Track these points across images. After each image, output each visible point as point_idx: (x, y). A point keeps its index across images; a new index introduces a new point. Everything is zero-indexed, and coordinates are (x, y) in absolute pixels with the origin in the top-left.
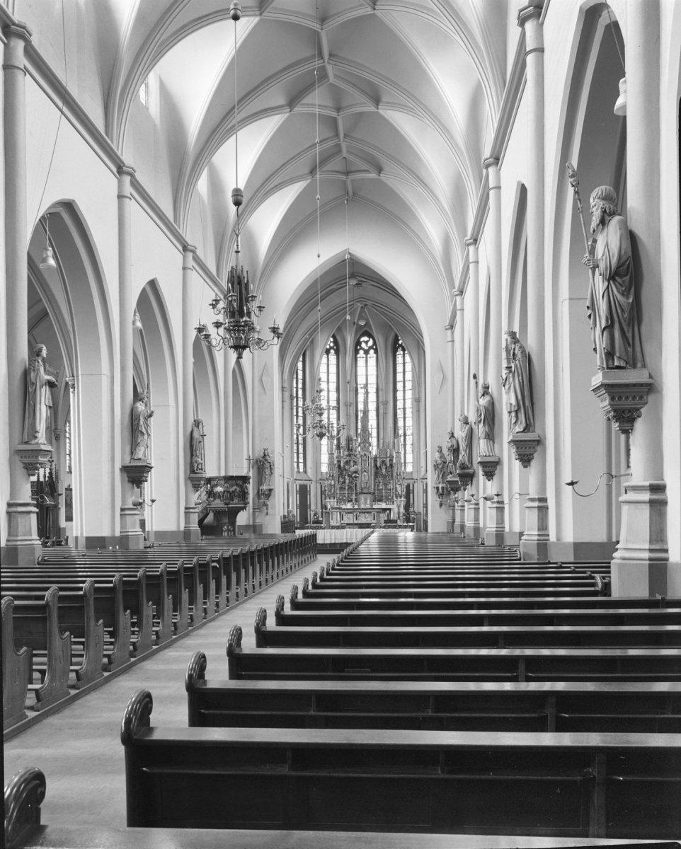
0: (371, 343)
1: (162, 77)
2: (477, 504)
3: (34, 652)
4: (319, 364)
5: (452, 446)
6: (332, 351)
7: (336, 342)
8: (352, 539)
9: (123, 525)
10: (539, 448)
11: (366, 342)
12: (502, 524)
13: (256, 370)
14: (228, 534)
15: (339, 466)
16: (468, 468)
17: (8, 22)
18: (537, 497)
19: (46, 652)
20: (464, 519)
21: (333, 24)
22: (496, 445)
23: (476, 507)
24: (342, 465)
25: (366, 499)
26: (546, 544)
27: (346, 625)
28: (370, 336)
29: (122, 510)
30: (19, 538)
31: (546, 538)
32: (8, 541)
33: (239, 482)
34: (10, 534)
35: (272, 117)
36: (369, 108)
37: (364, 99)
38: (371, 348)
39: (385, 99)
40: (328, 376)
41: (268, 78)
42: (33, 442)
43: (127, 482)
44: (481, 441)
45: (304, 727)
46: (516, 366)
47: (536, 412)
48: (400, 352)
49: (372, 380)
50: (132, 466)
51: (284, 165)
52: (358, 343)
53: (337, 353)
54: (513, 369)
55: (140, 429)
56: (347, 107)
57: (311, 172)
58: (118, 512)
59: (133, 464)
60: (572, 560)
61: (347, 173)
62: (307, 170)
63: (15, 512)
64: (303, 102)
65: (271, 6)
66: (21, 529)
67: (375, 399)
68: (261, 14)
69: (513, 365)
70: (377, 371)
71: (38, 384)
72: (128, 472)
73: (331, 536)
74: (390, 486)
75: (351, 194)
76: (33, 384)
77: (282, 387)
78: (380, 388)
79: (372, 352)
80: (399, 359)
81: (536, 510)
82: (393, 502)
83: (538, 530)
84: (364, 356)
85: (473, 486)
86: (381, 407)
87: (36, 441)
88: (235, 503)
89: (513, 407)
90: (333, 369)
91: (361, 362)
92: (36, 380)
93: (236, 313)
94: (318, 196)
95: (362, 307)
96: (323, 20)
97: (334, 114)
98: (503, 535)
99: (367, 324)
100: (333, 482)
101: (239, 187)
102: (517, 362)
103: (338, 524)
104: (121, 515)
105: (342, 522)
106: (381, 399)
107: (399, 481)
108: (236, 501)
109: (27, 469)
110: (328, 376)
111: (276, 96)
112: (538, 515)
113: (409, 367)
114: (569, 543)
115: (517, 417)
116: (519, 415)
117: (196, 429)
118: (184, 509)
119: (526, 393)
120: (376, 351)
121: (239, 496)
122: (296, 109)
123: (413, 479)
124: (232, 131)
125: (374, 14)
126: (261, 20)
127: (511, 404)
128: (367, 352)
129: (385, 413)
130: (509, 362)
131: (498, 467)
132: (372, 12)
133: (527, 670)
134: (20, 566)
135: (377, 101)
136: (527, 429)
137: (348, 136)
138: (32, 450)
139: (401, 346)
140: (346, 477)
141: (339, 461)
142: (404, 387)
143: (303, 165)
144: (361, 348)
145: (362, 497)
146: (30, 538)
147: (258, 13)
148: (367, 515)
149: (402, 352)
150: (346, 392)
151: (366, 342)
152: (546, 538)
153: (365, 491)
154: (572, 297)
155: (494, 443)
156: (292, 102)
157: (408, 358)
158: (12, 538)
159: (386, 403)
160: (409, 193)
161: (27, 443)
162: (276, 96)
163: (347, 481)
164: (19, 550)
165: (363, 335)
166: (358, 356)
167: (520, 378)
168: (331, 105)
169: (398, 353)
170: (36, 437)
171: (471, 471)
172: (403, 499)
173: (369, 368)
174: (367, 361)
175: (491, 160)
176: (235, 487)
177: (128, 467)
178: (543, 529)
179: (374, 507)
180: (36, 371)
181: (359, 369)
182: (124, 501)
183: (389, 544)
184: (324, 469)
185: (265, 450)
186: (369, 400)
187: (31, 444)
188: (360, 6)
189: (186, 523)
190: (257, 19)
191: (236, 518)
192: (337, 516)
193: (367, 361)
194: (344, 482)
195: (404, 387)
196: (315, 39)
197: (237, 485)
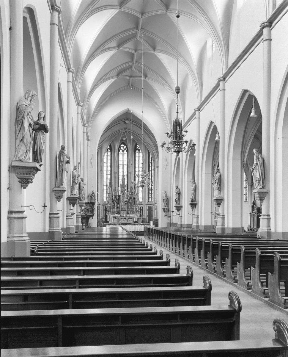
0: (125, 147)
1: (207, 41)
2: (182, 217)
3: (261, 275)
4: (104, 155)
5: (178, 192)
6: (109, 150)
7: (110, 146)
8: (137, 229)
9: (67, 223)
10: (267, 195)
11: (123, 147)
12: (224, 224)
13: (89, 157)
14: (85, 227)
15: (112, 199)
16: (194, 201)
17: (55, 5)
18: (266, 214)
19: (265, 275)
20: (198, 222)
21: (146, 16)
22: (221, 193)
23: (268, 217)
24: (114, 198)
25: (124, 213)
26: (270, 233)
27: (139, 266)
28: (125, 144)
29: (67, 216)
30: (55, 228)
31: (270, 230)
32: (49, 229)
33: (91, 205)
34: (50, 227)
35: (109, 52)
36: (151, 51)
37: (150, 47)
38: (125, 149)
39: (158, 48)
40: (107, 160)
41: (115, 35)
42: (61, 187)
43: (69, 204)
44: (216, 191)
45: (206, 305)
46: (260, 163)
47: (266, 181)
48: (137, 151)
49: (125, 163)
50: (72, 198)
51: (110, 71)
52: (120, 147)
53: (111, 151)
54: (258, 164)
55: (75, 182)
56: (140, 50)
57: (117, 75)
58: (65, 217)
59: (72, 196)
60: (282, 239)
61: (131, 77)
62: (116, 74)
63: (53, 217)
64: (124, 46)
65: (125, 6)
66: (55, 225)
67: (126, 171)
68: (120, 9)
69: (258, 162)
70: (128, 159)
71: (64, 162)
72: (69, 200)
73: (132, 228)
74: (134, 207)
75: (130, 85)
76: (62, 162)
77: (158, 168)
78: (129, 166)
79: (125, 151)
80: (137, 155)
81: (266, 219)
82: (135, 214)
83: (267, 227)
84: (122, 153)
85: (196, 208)
86: (129, 174)
87: (62, 186)
88: (89, 214)
89: (258, 179)
90: (109, 157)
91: (121, 155)
92: (63, 160)
93: (178, 138)
94: (143, 87)
95: (124, 132)
96: (142, 14)
97: (134, 52)
98: (224, 228)
99: (126, 140)
100: (110, 205)
101: (178, 86)
102: (260, 161)
103: (112, 223)
104: (67, 218)
105: (114, 222)
106: (129, 171)
107: (137, 205)
108: (89, 213)
109: (57, 199)
110: (107, 160)
111: (114, 44)
112: (267, 221)
113: (141, 158)
114: (281, 232)
115: (259, 183)
116: (260, 182)
117: (81, 182)
118: (7, 213)
119: (263, 174)
120: (127, 151)
121: (91, 211)
122: (121, 49)
123: (142, 205)
124: (97, 55)
125: (166, 14)
126: (120, 11)
127: (257, 178)
128: (123, 151)
129: (131, 177)
130: (257, 161)
131: (222, 202)
132: (166, 13)
133: (80, 284)
134: (55, 240)
135: (154, 48)
136: (263, 188)
137: (137, 61)
138: (61, 190)
139: (138, 149)
140: (115, 203)
141: (112, 197)
142: (139, 166)
143: (115, 73)
144: (121, 149)
145: (122, 212)
146: (58, 228)
147: (119, 8)
148: (124, 219)
149: (138, 152)
150: (115, 167)
151: (123, 147)
152: (270, 230)
153: (123, 209)
154: (284, 137)
155: (221, 192)
156: (119, 46)
157: (141, 154)
158: (51, 228)
159: (131, 173)
160: (156, 86)
161: (58, 187)
162: (114, 44)
163: (116, 205)
164: (55, 234)
165: (122, 144)
166: (120, 152)
167: (261, 167)
168: (133, 48)
169: (136, 152)
170: (62, 185)
171: (196, 202)
172: (139, 213)
173: (124, 158)
174: (123, 155)
175: (222, 79)
176: (89, 207)
177: (70, 198)
178: (269, 227)
179: (127, 216)
180: (63, 156)
181: (120, 158)
182: (67, 213)
183: (114, 232)
184: (105, 200)
185: (92, 191)
186: (123, 171)
187: (60, 188)
188: (161, 10)
189: (77, 222)
190: (118, 10)
191: (88, 220)
192: (184, 221)
193: (123, 155)
194: (114, 205)
195: (139, 166)
196: (136, 21)
197: (90, 206)
